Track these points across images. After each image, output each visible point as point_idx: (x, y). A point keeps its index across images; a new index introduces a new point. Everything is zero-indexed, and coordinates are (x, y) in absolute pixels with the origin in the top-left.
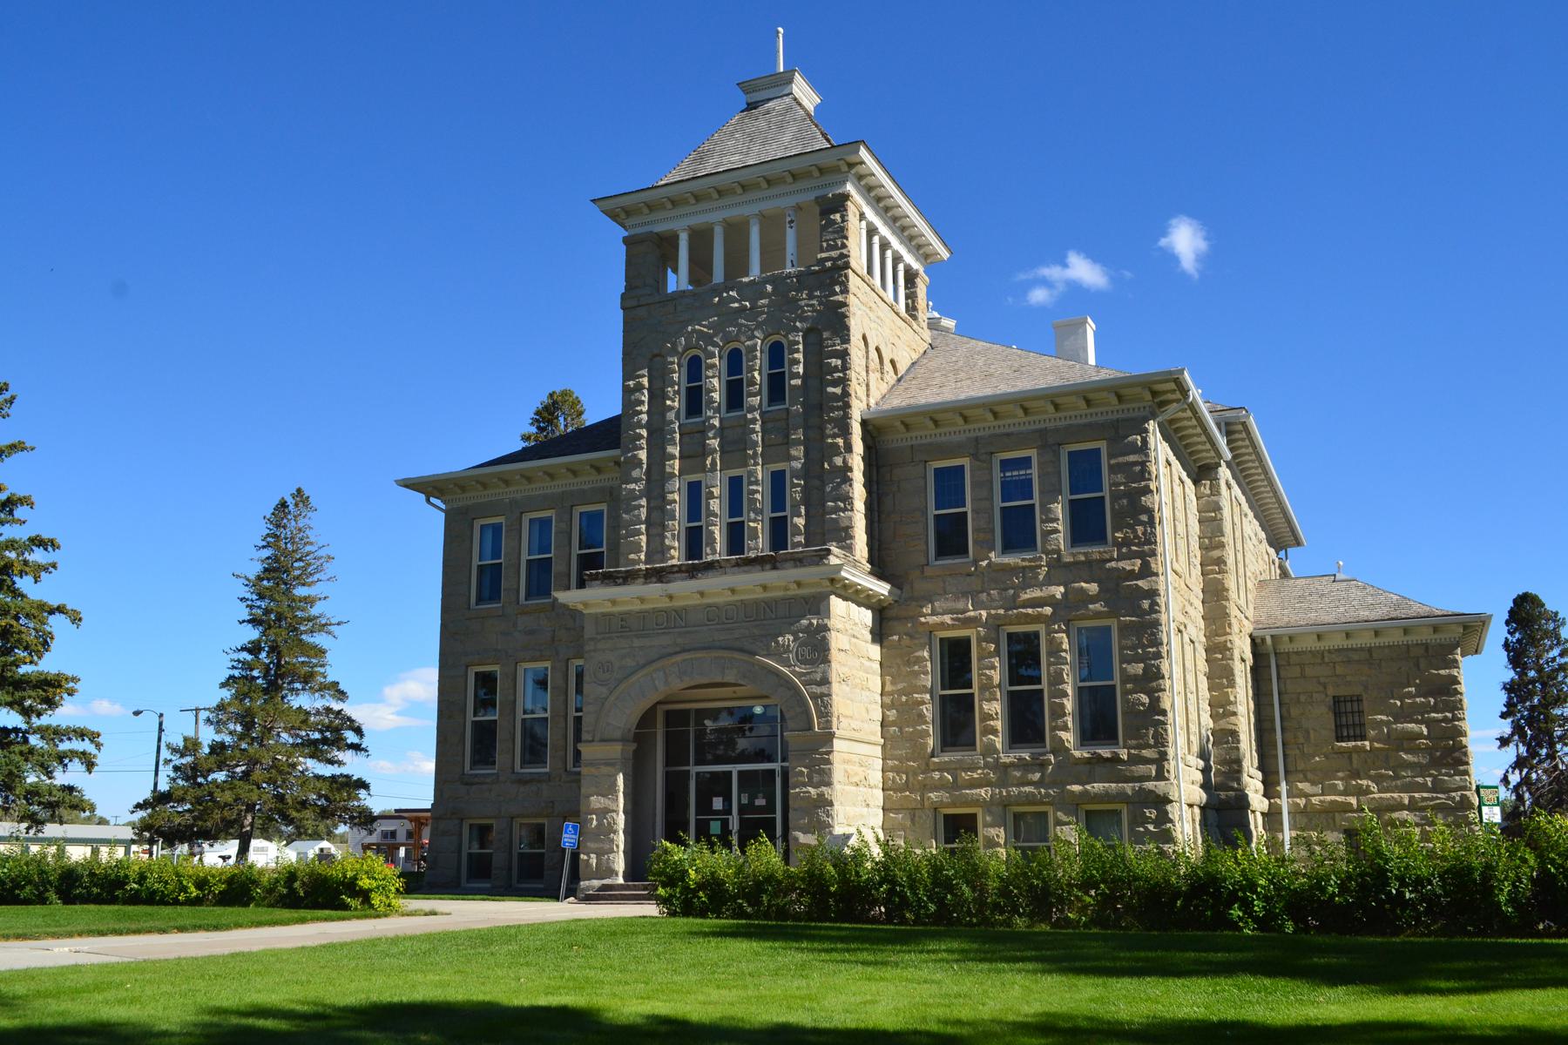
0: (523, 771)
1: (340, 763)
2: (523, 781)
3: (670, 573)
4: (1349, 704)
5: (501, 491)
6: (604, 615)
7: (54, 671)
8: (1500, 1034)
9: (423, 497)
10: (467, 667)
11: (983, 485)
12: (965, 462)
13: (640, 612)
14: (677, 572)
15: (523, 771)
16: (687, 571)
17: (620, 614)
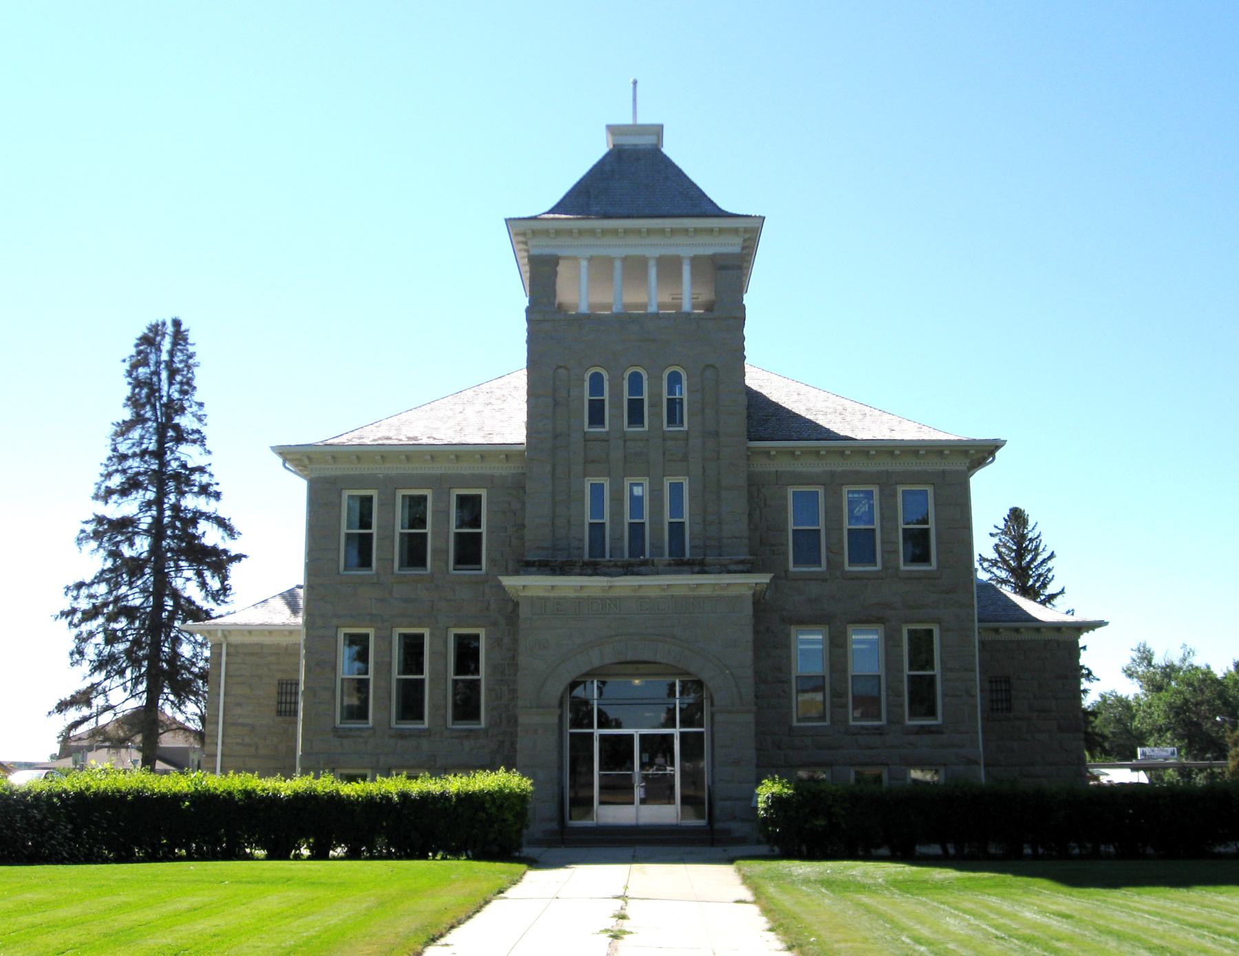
0: (454, 727)
1: (1107, 774)
2: (402, 735)
3: (605, 566)
4: (1000, 707)
5: (378, 466)
6: (539, 598)
7: (1233, 666)
8: (568, 866)
9: (280, 461)
10: (337, 627)
11: (442, 514)
12: (428, 492)
13: (577, 598)
14: (612, 566)
15: (454, 727)
16: (622, 567)
17: (555, 598)
